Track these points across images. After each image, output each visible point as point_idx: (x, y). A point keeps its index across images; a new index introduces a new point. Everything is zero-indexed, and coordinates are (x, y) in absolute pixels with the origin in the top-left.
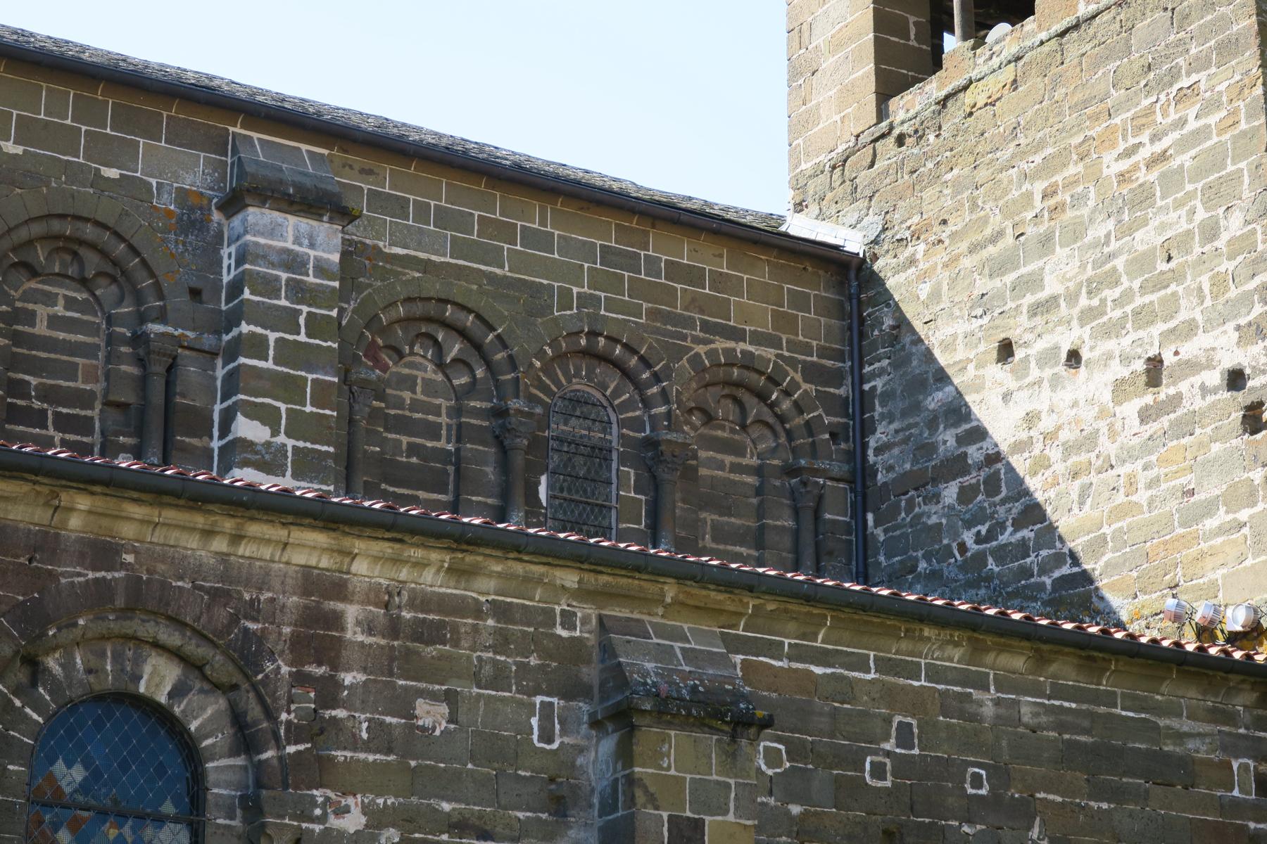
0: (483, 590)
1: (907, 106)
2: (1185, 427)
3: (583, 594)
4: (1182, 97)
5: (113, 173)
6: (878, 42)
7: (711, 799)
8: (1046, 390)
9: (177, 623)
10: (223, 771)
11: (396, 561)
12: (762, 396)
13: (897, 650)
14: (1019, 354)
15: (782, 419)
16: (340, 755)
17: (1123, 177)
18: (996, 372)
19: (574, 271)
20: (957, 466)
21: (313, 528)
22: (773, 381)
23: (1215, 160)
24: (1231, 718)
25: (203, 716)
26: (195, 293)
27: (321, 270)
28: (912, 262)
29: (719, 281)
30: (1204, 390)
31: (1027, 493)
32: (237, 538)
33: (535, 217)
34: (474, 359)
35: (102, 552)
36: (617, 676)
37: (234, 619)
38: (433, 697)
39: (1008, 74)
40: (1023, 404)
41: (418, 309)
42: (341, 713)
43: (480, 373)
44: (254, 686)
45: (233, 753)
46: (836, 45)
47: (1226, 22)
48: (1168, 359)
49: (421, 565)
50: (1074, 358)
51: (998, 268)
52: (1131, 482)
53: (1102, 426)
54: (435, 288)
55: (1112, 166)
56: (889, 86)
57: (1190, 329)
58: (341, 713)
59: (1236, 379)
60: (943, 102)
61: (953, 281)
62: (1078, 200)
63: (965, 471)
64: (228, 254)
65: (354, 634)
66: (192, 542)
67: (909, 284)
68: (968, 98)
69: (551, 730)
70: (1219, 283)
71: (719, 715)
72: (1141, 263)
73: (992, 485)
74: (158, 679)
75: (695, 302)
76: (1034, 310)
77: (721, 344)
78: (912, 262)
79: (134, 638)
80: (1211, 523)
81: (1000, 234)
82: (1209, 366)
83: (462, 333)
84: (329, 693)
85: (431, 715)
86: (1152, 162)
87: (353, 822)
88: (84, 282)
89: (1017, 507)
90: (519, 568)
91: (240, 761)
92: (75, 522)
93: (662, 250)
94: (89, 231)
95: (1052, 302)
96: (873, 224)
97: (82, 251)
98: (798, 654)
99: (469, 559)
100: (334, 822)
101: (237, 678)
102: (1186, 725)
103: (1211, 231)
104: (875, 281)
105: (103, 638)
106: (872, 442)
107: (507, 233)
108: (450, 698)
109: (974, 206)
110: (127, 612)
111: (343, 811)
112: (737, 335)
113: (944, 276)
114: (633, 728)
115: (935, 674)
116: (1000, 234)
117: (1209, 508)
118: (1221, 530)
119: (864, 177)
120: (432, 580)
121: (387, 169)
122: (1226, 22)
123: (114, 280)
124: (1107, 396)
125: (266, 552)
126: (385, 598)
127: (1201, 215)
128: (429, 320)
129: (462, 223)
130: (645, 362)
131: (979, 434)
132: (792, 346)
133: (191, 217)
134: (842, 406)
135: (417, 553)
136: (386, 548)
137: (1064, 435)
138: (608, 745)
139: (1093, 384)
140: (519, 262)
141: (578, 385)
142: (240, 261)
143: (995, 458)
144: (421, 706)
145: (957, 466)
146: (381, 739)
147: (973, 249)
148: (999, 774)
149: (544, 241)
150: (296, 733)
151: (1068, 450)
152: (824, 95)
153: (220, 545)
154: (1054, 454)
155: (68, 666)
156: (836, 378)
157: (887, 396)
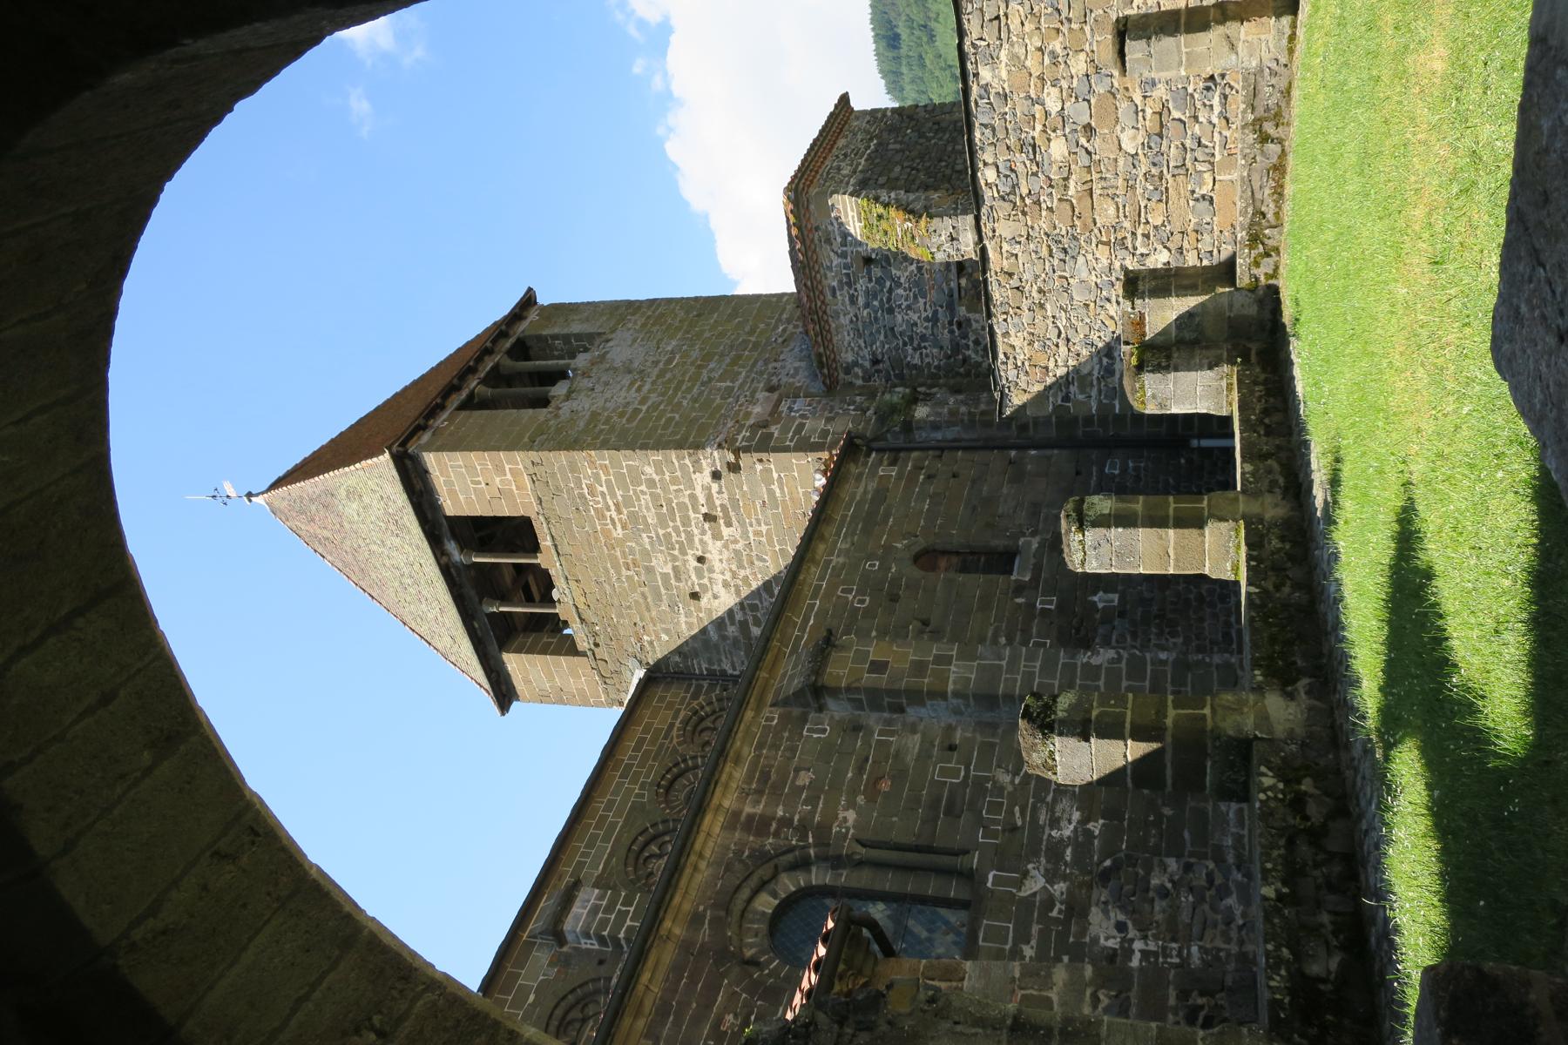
0: (748, 753)
1: (583, 644)
2: (734, 502)
3: (758, 710)
4: (592, 493)
5: (532, 997)
6: (552, 653)
7: (861, 657)
8: (714, 576)
9: (738, 888)
10: (818, 876)
11: (726, 786)
12: (702, 719)
13: (808, 591)
14: (697, 589)
15: (714, 712)
16: (817, 818)
17: (624, 528)
18: (704, 601)
19: (630, 791)
20: (744, 626)
21: (702, 819)
22: (696, 713)
23: (620, 478)
24: (861, 474)
25: (788, 884)
26: (601, 962)
27: (601, 898)
28: (651, 643)
29: (646, 731)
30: (720, 492)
31: (758, 589)
32: (701, 856)
33: (599, 805)
34: (660, 840)
35: (696, 920)
36: (798, 694)
37: (741, 861)
38: (795, 777)
39: (573, 584)
40: (718, 588)
41: (631, 860)
42: (797, 818)
43: (667, 838)
44: (777, 856)
45: (810, 872)
46: (550, 677)
47: (561, 468)
48: (704, 510)
49: (730, 776)
50: (701, 560)
51: (658, 597)
52: (757, 533)
53: (732, 546)
54: (623, 852)
55: (619, 532)
56: (569, 648)
57: (693, 497)
58: (797, 818)
59: (716, 476)
60: (582, 620)
61: (662, 621)
62: (632, 551)
63: (746, 622)
64: (586, 944)
65: (759, 809)
66: (699, 878)
67: (661, 645)
68: (581, 606)
69: (820, 729)
70: (674, 481)
71: (823, 650)
72: (662, 522)
73: (754, 608)
74: (766, 904)
75: (653, 742)
76: (678, 579)
77: (675, 732)
78: (651, 643)
79: (744, 911)
80: (778, 494)
81: (643, 594)
82: (709, 488)
83: (647, 844)
84: (786, 822)
85: (804, 779)
86: (619, 512)
87: (851, 816)
88: (584, 1020)
89: (764, 595)
90: (740, 735)
91: (814, 869)
92: (677, 931)
93: (626, 755)
94: (559, 1012)
95: (675, 568)
96: (632, 663)
97: (569, 1018)
98: (803, 629)
99: (732, 754)
100: (850, 823)
101: (771, 864)
102: (861, 490)
103: (651, 483)
104: (658, 663)
105: (740, 927)
106: (730, 671)
107: (603, 818)
108: (797, 771)
109: (629, 607)
110: (728, 911)
111: (845, 820)
112: (672, 726)
113: (659, 626)
114: (823, 687)
115: (822, 578)
116: (643, 594)
117: (771, 493)
118: (782, 489)
119: (611, 666)
120: (740, 774)
121: (562, 868)
122: (561, 468)
123: (586, 1005)
124: (719, 544)
125: (711, 844)
126: (744, 794)
127: (643, 488)
128: (637, 859)
129: (594, 837)
130: (677, 764)
131: (730, 612)
132: (682, 703)
133: (563, 962)
134: (712, 687)
135: (724, 777)
136: (719, 790)
137: (734, 567)
138: (831, 703)
139: (715, 551)
140: (618, 814)
141: (682, 796)
142: (588, 936)
143: (741, 604)
144: (799, 783)
145: (744, 626)
146: (813, 800)
147: (648, 610)
148: (871, 557)
149: (611, 803)
150: (804, 837)
151: (741, 566)
152: (572, 685)
153: (703, 865)
154: (742, 573)
155: (751, 946)
156: (699, 687)
157: (710, 662)
